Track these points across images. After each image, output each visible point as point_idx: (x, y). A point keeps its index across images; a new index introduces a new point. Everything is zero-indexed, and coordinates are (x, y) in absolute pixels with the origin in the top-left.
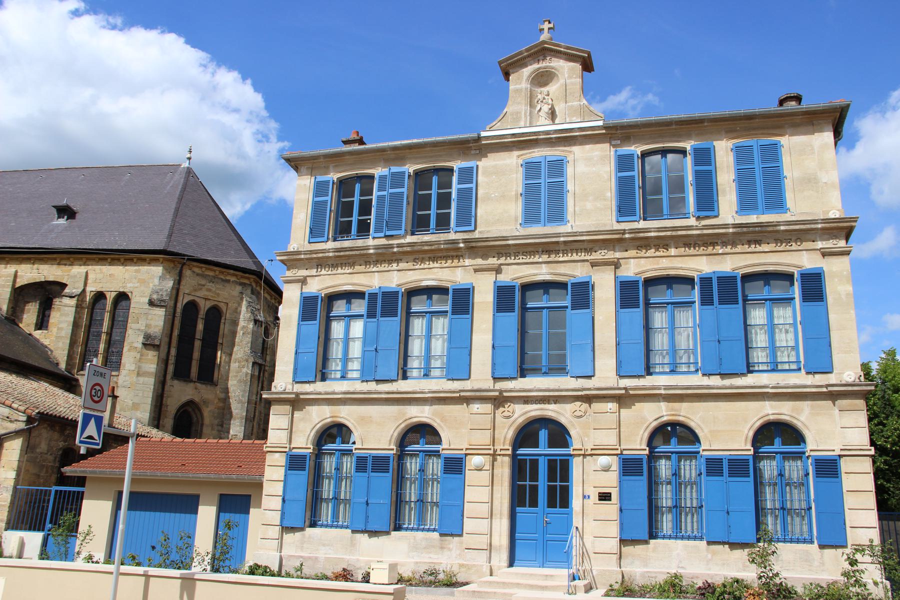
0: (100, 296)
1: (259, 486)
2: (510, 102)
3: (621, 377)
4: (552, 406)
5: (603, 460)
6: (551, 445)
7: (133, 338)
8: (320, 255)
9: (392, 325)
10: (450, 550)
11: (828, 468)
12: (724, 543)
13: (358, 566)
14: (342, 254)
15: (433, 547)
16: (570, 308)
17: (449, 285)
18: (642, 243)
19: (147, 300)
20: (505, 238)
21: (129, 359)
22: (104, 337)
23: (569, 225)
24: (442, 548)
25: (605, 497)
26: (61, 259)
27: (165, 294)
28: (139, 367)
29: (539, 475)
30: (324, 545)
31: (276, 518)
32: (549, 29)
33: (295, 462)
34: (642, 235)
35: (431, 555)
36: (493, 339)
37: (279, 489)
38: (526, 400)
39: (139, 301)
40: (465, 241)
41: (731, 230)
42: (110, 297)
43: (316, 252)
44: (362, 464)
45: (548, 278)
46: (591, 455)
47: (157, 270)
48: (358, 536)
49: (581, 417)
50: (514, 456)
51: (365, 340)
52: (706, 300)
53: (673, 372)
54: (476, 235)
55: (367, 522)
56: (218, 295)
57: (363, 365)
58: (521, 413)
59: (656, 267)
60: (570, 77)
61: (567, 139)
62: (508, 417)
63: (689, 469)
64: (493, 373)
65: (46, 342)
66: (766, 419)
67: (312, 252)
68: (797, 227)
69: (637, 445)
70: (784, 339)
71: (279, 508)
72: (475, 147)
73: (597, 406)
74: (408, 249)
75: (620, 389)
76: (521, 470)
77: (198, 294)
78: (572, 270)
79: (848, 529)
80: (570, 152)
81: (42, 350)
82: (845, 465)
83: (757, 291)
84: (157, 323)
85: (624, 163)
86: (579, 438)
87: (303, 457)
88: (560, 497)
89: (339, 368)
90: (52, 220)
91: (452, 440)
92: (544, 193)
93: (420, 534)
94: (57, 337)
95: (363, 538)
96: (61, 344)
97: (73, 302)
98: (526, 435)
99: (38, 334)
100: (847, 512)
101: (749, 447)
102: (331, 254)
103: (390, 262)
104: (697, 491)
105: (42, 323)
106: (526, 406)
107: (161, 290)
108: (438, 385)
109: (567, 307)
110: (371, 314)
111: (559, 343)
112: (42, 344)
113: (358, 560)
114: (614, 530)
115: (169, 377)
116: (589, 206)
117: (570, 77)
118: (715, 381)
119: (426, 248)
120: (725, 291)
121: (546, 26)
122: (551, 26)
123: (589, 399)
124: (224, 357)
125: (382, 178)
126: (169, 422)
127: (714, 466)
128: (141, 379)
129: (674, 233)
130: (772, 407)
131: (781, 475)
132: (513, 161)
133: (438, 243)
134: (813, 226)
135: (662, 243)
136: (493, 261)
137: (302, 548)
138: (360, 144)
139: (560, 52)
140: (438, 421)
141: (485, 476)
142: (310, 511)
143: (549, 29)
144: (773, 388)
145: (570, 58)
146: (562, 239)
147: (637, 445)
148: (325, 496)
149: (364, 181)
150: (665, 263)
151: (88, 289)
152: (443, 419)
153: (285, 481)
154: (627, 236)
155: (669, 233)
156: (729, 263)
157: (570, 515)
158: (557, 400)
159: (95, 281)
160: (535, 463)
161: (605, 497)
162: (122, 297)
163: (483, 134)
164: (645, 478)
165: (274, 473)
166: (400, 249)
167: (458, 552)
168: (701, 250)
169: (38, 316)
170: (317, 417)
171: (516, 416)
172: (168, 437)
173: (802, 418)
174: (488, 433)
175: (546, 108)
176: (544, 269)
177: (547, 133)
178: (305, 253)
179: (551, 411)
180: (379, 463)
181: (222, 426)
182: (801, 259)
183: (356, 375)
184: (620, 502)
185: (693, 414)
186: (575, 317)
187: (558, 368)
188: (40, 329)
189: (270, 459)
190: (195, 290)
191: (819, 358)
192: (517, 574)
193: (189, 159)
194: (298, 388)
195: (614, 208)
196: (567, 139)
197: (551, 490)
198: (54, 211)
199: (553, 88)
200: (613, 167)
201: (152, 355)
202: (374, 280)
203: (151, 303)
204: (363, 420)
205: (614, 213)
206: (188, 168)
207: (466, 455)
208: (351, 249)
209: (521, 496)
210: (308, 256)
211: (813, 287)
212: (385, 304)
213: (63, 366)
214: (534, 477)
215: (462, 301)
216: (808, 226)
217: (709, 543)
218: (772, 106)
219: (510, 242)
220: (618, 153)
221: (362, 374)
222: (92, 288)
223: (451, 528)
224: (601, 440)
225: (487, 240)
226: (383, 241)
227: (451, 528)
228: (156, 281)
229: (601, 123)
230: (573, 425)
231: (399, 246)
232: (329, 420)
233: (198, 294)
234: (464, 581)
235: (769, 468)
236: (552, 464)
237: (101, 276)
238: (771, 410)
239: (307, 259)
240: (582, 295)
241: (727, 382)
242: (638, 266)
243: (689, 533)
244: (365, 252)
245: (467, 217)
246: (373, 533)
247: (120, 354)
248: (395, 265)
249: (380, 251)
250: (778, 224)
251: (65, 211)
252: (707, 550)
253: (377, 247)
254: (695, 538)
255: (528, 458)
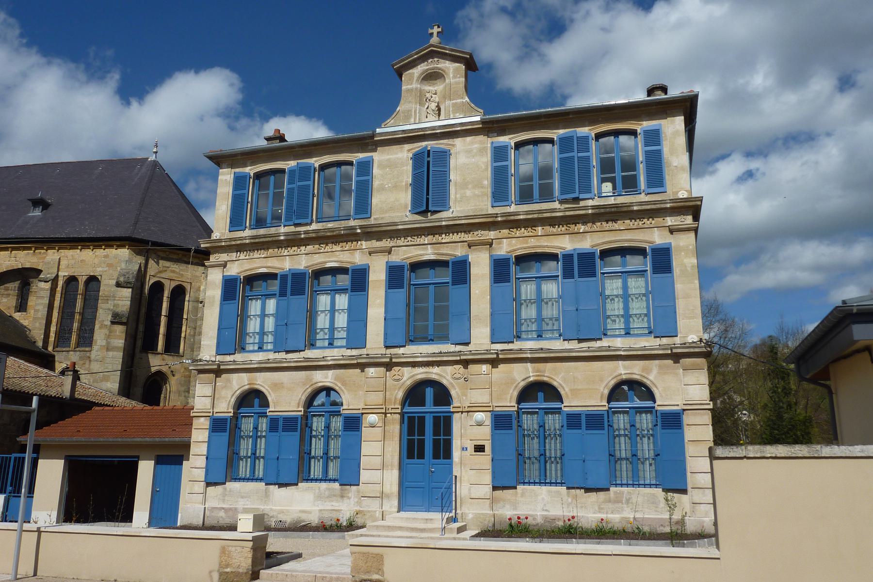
0: (72, 280)
1: (187, 446)
2: (402, 102)
3: (492, 343)
4: (436, 370)
5: (479, 416)
6: (437, 403)
7: (103, 316)
8: (239, 242)
9: (298, 303)
10: (349, 498)
11: (672, 421)
12: (275, 484)
13: (271, 515)
14: (257, 240)
15: (334, 496)
16: (450, 284)
17: (558, 251)
18: (512, 223)
19: (114, 282)
20: (395, 224)
21: (99, 336)
22: (77, 317)
23: (451, 210)
24: (342, 497)
25: (479, 449)
26: (36, 248)
27: (131, 276)
28: (108, 343)
29: (426, 429)
30: (242, 497)
31: (201, 474)
32: (438, 33)
33: (217, 425)
34: (512, 218)
35: (333, 503)
36: (385, 313)
37: (203, 449)
38: (414, 365)
39: (107, 285)
40: (361, 227)
41: (590, 211)
42: (82, 280)
43: (235, 239)
44: (274, 424)
45: (433, 257)
46: (468, 412)
47: (124, 253)
48: (272, 487)
49: (459, 379)
50: (402, 414)
51: (277, 316)
52: (568, 273)
53: (540, 336)
54: (372, 221)
55: (278, 475)
56: (182, 275)
57: (275, 339)
58: (409, 376)
59: (525, 245)
60: (454, 77)
61: (451, 133)
62: (398, 380)
63: (553, 422)
64: (385, 342)
65: (25, 323)
66: (619, 378)
67: (231, 239)
68: (649, 207)
69: (508, 403)
70: (637, 307)
71: (204, 465)
72: (369, 143)
73: (473, 368)
74: (314, 235)
75: (492, 353)
76: (412, 427)
77: (163, 275)
78: (452, 248)
79: (689, 474)
80: (453, 145)
81: (21, 330)
82: (687, 419)
83: (616, 264)
84: (124, 303)
85: (499, 153)
86: (459, 397)
87: (224, 420)
88: (443, 450)
89: (257, 341)
90: (29, 212)
91: (350, 402)
92: (430, 181)
93: (324, 485)
94: (34, 319)
95: (274, 489)
96: (37, 325)
97: (48, 286)
98: (415, 394)
99: (17, 316)
100: (688, 459)
101: (514, 404)
102: (247, 241)
103: (299, 246)
104: (654, 443)
105: (22, 306)
106: (414, 369)
107: (128, 273)
108: (334, 354)
109: (448, 283)
110: (283, 294)
111: (442, 313)
112: (22, 325)
113: (271, 509)
114: (487, 478)
115: (137, 350)
116: (468, 193)
117: (454, 77)
118: (574, 345)
119: (329, 234)
120: (582, 265)
121: (436, 30)
122: (440, 30)
123: (466, 363)
124: (188, 331)
125: (292, 171)
126: (139, 390)
127: (573, 420)
128: (111, 354)
129: (540, 216)
130: (625, 367)
131: (633, 426)
132: (404, 154)
133: (338, 229)
134: (663, 206)
135: (530, 223)
136: (386, 243)
137: (224, 501)
138: (280, 141)
139: (446, 54)
140: (339, 385)
141: (378, 431)
142: (225, 469)
143: (438, 33)
144: (624, 351)
145: (455, 59)
146: (444, 223)
147: (508, 403)
148: (243, 453)
149: (278, 175)
150: (533, 242)
151: (60, 273)
152: (344, 383)
153: (209, 442)
154: (499, 219)
155: (536, 216)
156: (589, 240)
157: (451, 464)
158: (439, 364)
159: (68, 267)
160: (422, 420)
161: (479, 449)
162: (93, 280)
163: (378, 130)
164: (298, 434)
165: (200, 437)
166: (307, 236)
167: (356, 500)
168: (563, 229)
169: (17, 300)
170: (239, 383)
171: (405, 378)
172: (140, 406)
173: (651, 377)
174: (381, 394)
175: (433, 106)
176: (430, 249)
177: (433, 128)
178: (226, 240)
179: (434, 373)
180: (289, 424)
181: (188, 392)
182: (654, 236)
183: (270, 347)
184: (492, 453)
185: (556, 375)
186: (455, 292)
187: (442, 337)
188: (19, 311)
189: (196, 423)
190: (160, 272)
191: (663, 321)
192: (402, 518)
193: (156, 152)
194: (219, 358)
195: (490, 194)
196: (451, 133)
197: (436, 443)
198: (30, 203)
199: (438, 87)
200: (489, 159)
201: (120, 330)
202: (286, 262)
203: (118, 285)
204: (276, 386)
205: (490, 199)
206: (154, 161)
207: (363, 414)
208: (265, 236)
209: (412, 449)
210: (228, 243)
211: (662, 260)
212: (296, 284)
213: (40, 344)
214: (422, 432)
215: (359, 280)
216: (658, 206)
217: (568, 488)
218: (640, 96)
219: (400, 227)
220: (495, 145)
221: (275, 346)
222: (64, 274)
223: (349, 477)
224: (479, 397)
225: (380, 225)
226: (292, 229)
227: (349, 477)
228: (123, 265)
229: (478, 119)
230: (453, 386)
231: (306, 232)
232: (247, 387)
233: (163, 275)
234: (360, 524)
235: (529, 422)
236: (436, 420)
237: (73, 262)
238: (624, 370)
239: (227, 246)
240: (460, 271)
241: (584, 345)
242: (509, 245)
243: (312, 476)
244: (277, 238)
245: (363, 206)
246: (281, 485)
247: (92, 331)
248: (303, 248)
249: (289, 238)
250: (631, 204)
251: (40, 203)
252: (568, 494)
253: (286, 234)
254: (556, 484)
255: (416, 415)
